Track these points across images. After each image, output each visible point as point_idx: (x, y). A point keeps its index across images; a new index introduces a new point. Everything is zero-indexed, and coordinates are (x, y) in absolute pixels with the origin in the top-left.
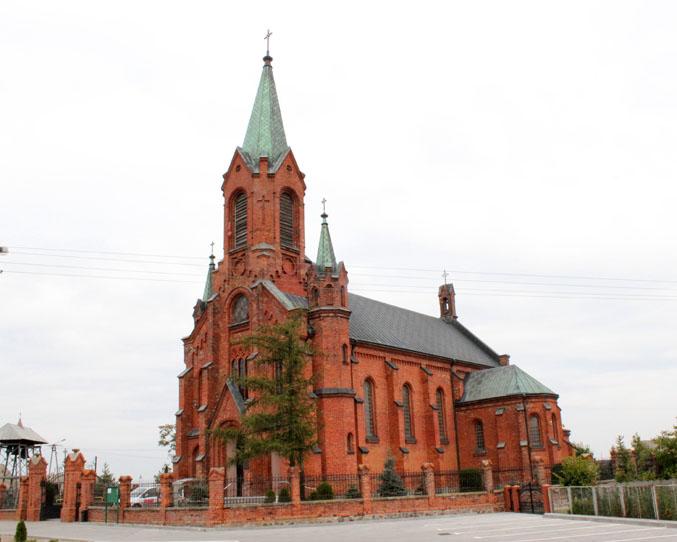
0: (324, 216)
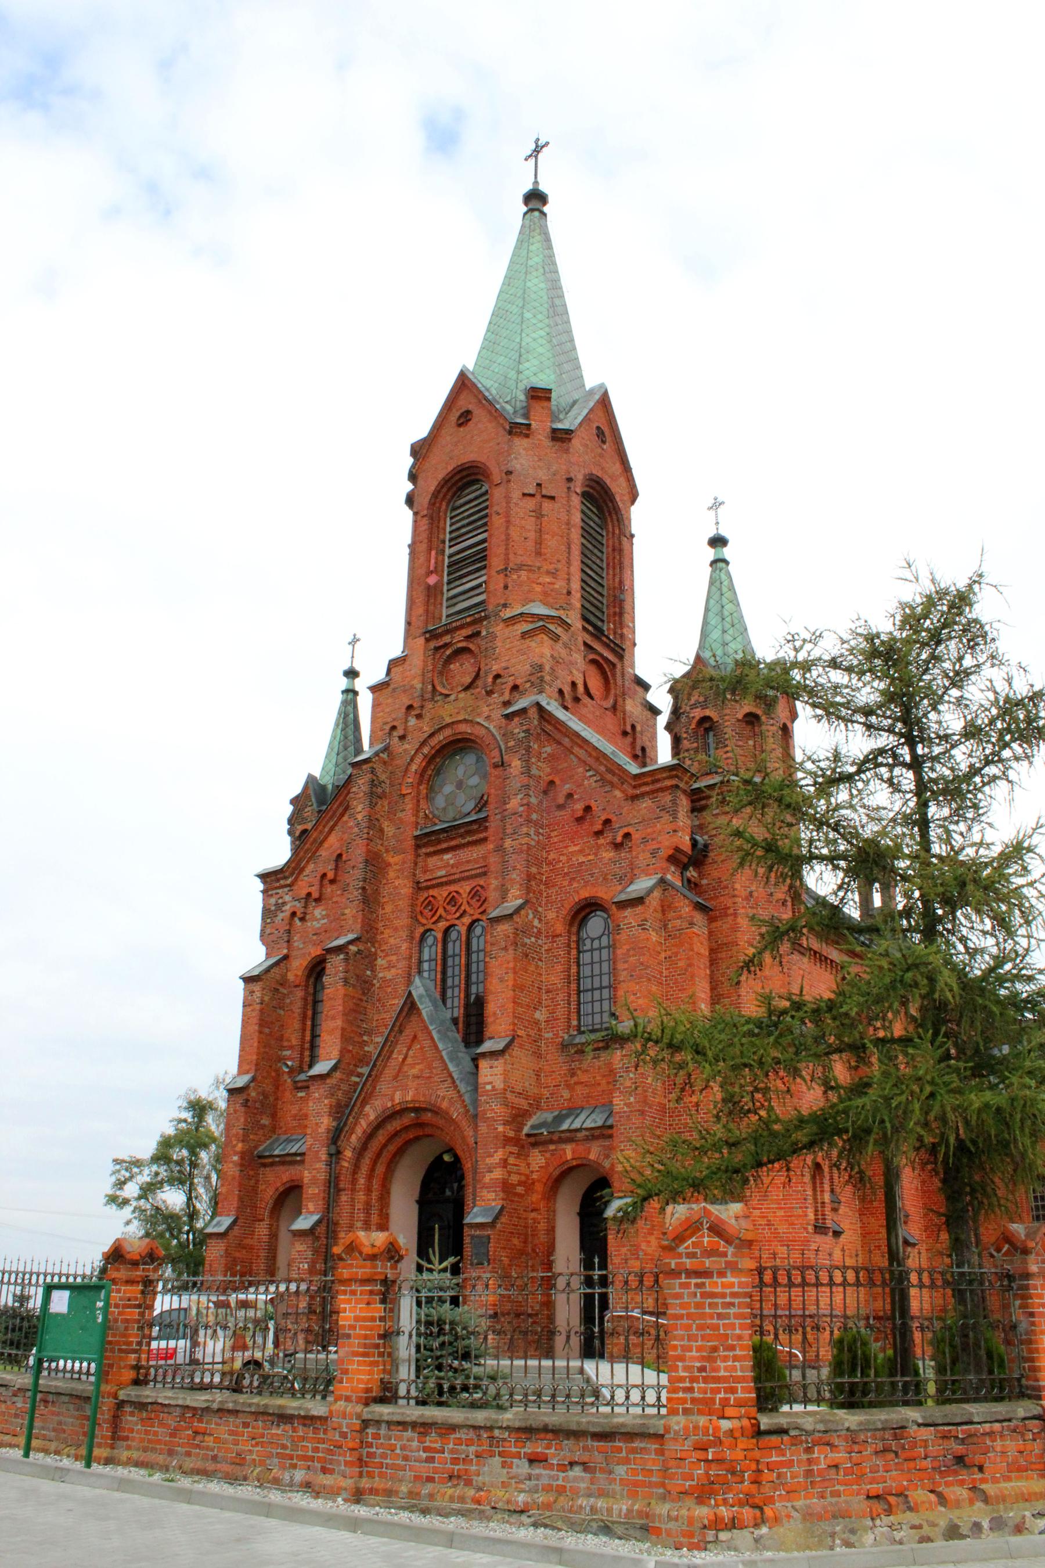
0: (718, 542)
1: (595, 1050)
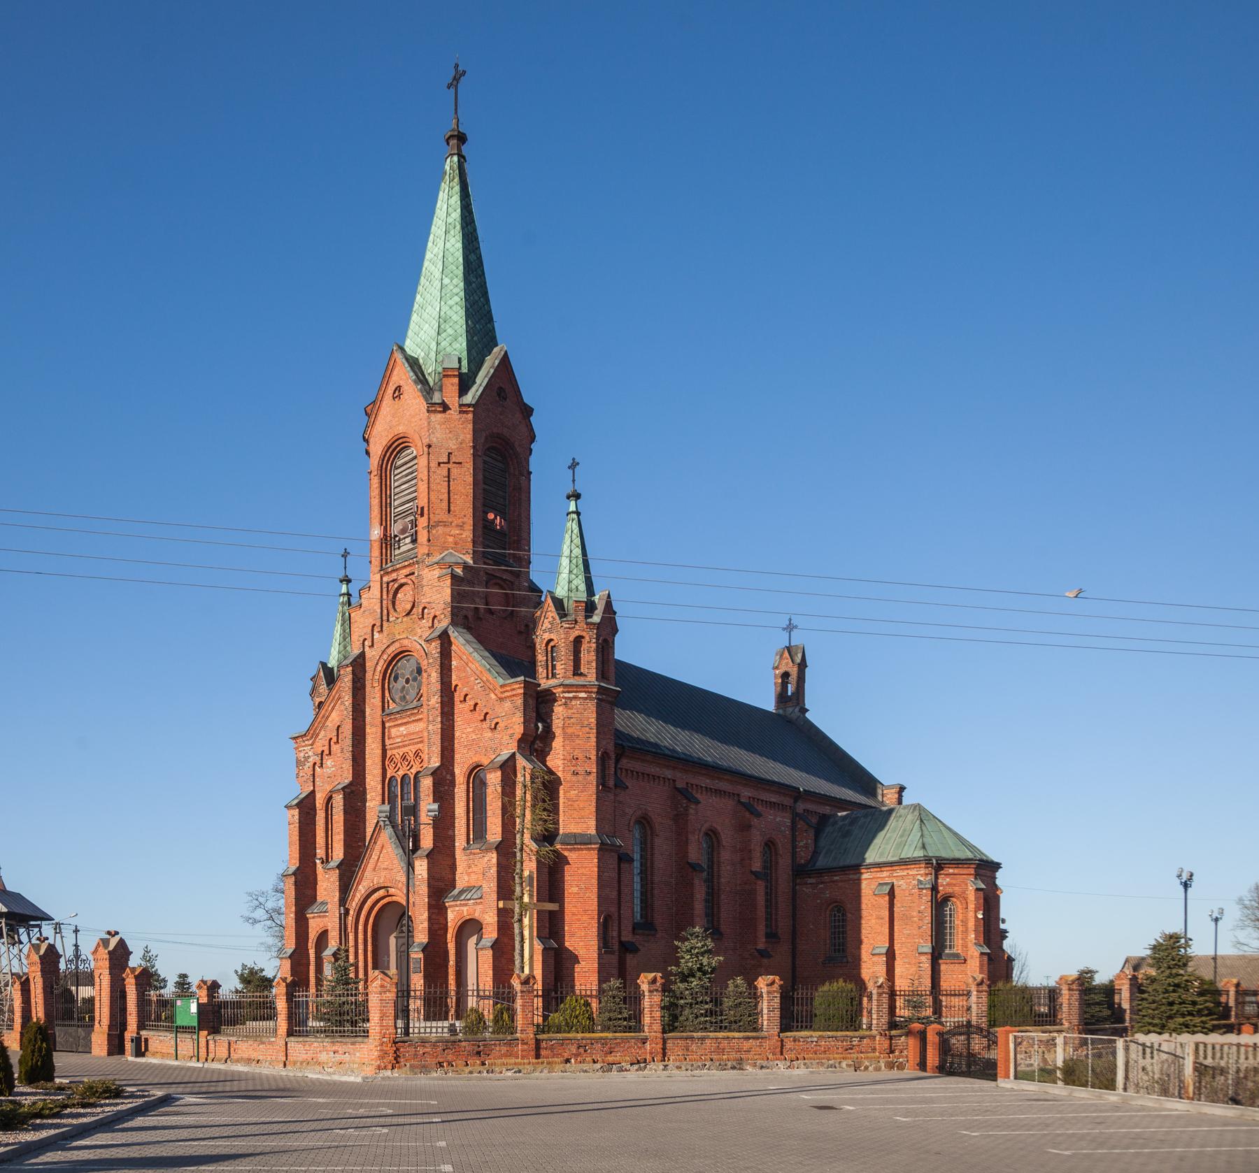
1: (786, 675)
